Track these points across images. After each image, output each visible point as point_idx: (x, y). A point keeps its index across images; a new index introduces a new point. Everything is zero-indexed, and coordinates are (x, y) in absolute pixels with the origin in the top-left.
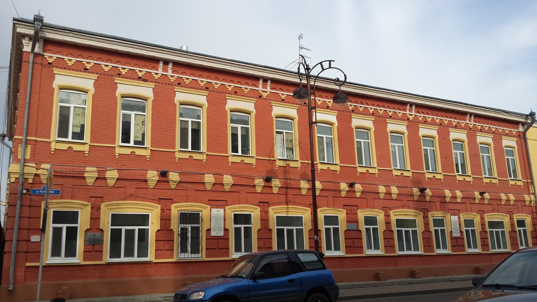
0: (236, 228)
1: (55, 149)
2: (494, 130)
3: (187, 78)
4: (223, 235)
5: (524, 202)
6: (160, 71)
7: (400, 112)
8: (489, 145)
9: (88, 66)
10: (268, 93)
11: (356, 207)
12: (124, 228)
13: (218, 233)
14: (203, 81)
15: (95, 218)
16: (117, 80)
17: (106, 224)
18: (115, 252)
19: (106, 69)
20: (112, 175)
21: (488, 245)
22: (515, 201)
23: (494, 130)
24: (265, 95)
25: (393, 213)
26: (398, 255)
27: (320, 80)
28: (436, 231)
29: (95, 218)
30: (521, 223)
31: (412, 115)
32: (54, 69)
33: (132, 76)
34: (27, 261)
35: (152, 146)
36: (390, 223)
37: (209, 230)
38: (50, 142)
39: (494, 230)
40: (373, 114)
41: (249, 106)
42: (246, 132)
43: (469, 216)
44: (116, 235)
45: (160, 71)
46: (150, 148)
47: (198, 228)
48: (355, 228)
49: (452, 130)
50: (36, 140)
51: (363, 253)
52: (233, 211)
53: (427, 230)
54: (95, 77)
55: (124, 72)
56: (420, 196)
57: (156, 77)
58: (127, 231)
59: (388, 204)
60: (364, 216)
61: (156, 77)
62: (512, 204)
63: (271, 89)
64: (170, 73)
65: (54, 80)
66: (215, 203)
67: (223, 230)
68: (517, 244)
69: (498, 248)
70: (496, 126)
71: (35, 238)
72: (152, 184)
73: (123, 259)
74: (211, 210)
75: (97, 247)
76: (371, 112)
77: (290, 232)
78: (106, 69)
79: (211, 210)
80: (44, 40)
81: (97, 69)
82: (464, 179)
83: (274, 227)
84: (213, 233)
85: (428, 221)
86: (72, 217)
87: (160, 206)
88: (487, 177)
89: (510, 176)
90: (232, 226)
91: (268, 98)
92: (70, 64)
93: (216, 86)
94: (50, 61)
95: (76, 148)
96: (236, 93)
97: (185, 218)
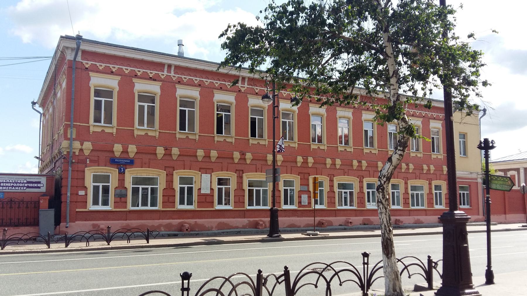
0: (94, 186)
1: (93, 132)
2: (424, 115)
3: (185, 78)
4: (209, 193)
5: (334, 166)
6: (165, 73)
7: (207, 80)
8: (155, 95)
9: (114, 70)
10: (246, 88)
11: (211, 170)
12: (141, 187)
13: (206, 191)
14: (197, 80)
15: (122, 181)
16: (134, 80)
17: (129, 185)
18: (135, 203)
19: (127, 72)
20: (214, 154)
21: (409, 204)
22: (435, 170)
23: (424, 115)
24: (243, 90)
25: (336, 178)
26: (337, 209)
27: (210, 65)
28: (436, 193)
29: (122, 181)
30: (438, 187)
31: (244, 87)
32: (90, 72)
33: (145, 77)
34: (77, 208)
35: (159, 129)
36: (333, 186)
37: (200, 189)
38: (338, 147)
39: (415, 192)
40: (413, 115)
41: (155, 88)
42: (192, 113)
43: (223, 175)
44: (135, 191)
45: (165, 73)
46: (159, 130)
47: (293, 190)
48: (306, 189)
49: (216, 91)
50: (79, 125)
51: (280, 208)
52: (217, 176)
53: (430, 193)
54: (119, 78)
55: (139, 74)
56: (358, 166)
57: (163, 77)
58: (256, 190)
59: (361, 173)
60: (92, 174)
61: (163, 77)
62: (328, 168)
63: (248, 85)
64: (172, 74)
65: (309, 110)
66: (208, 170)
67: (210, 189)
68: (433, 203)
69: (417, 206)
70: (426, 111)
71: (82, 193)
72: (160, 156)
73: (141, 208)
74: (201, 175)
75: (123, 199)
76: (411, 114)
77: (258, 192)
78: (127, 72)
79: (201, 175)
80: (82, 51)
81: (119, 73)
82: (225, 140)
83: (246, 188)
84: (203, 192)
85: (407, 186)
86: (106, 178)
87: (299, 177)
88: (145, 128)
89: (434, 151)
90: (216, 187)
91: (245, 92)
92: (101, 68)
93: (207, 84)
94: (87, 66)
95: (107, 130)
96: (221, 88)
97: (183, 180)
